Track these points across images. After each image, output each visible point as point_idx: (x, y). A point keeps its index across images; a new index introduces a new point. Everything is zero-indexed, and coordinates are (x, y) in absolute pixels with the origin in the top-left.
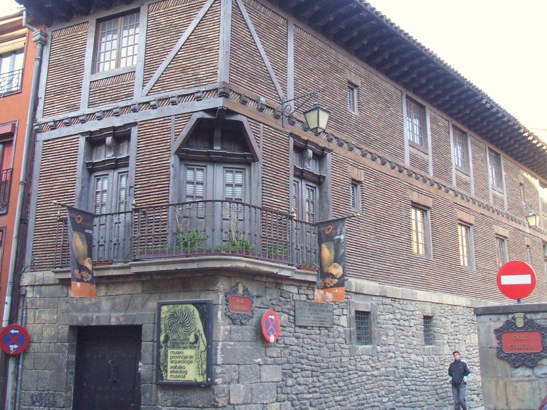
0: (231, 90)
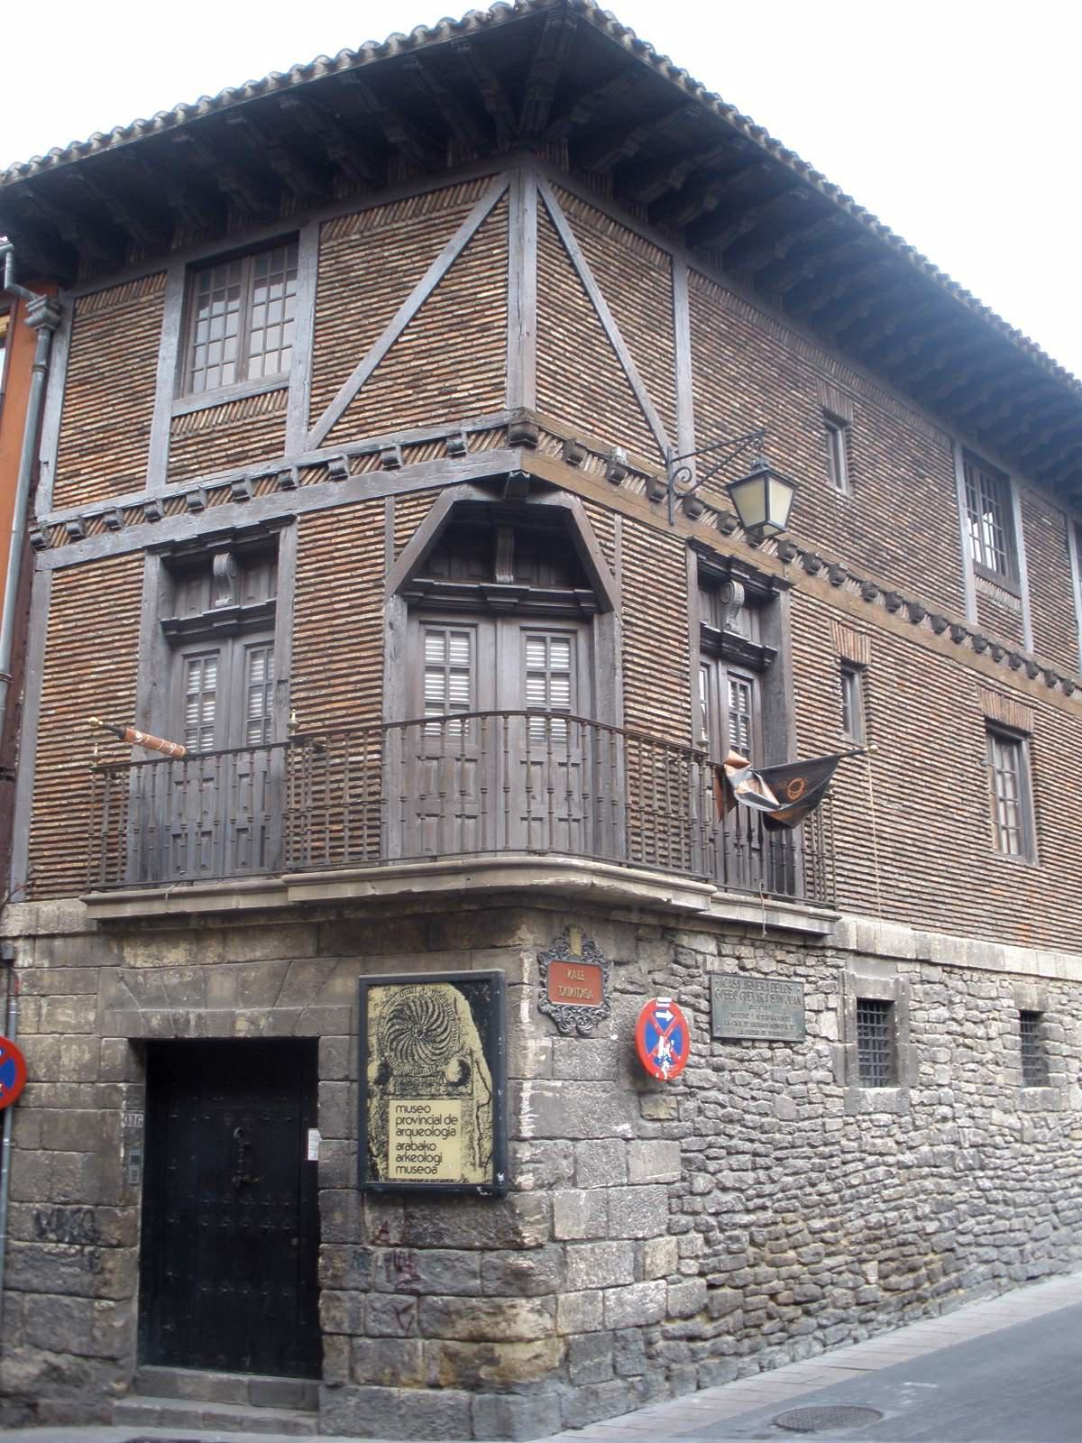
0: (541, 430)
